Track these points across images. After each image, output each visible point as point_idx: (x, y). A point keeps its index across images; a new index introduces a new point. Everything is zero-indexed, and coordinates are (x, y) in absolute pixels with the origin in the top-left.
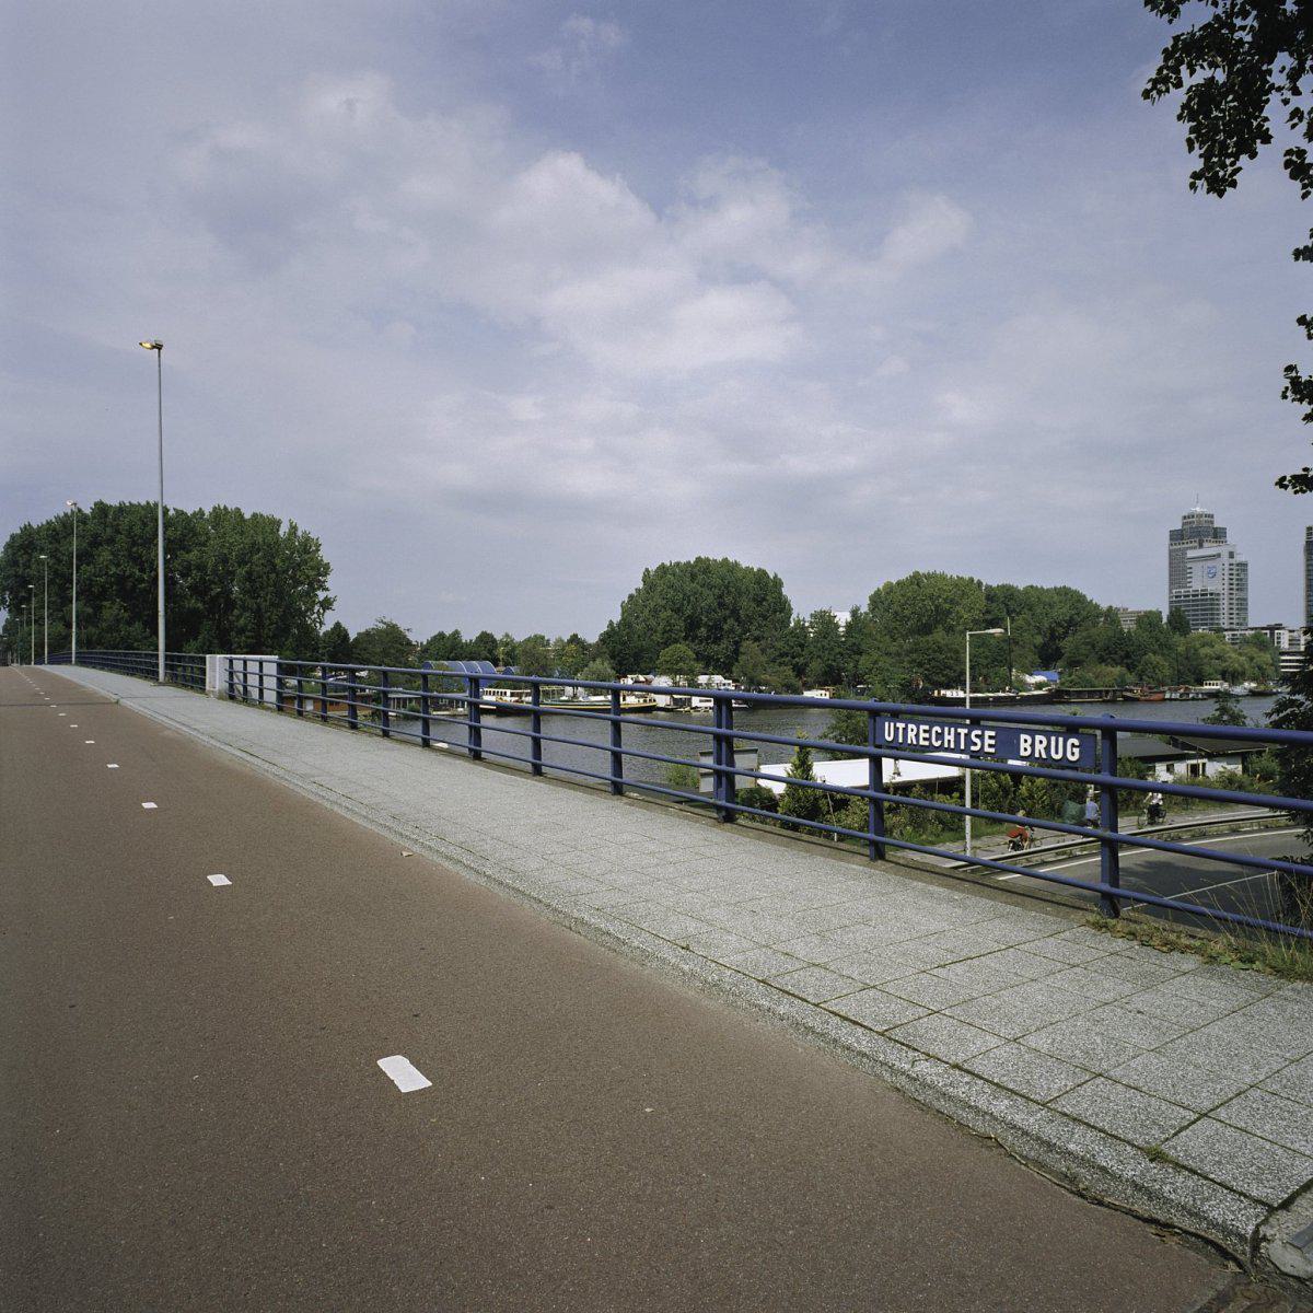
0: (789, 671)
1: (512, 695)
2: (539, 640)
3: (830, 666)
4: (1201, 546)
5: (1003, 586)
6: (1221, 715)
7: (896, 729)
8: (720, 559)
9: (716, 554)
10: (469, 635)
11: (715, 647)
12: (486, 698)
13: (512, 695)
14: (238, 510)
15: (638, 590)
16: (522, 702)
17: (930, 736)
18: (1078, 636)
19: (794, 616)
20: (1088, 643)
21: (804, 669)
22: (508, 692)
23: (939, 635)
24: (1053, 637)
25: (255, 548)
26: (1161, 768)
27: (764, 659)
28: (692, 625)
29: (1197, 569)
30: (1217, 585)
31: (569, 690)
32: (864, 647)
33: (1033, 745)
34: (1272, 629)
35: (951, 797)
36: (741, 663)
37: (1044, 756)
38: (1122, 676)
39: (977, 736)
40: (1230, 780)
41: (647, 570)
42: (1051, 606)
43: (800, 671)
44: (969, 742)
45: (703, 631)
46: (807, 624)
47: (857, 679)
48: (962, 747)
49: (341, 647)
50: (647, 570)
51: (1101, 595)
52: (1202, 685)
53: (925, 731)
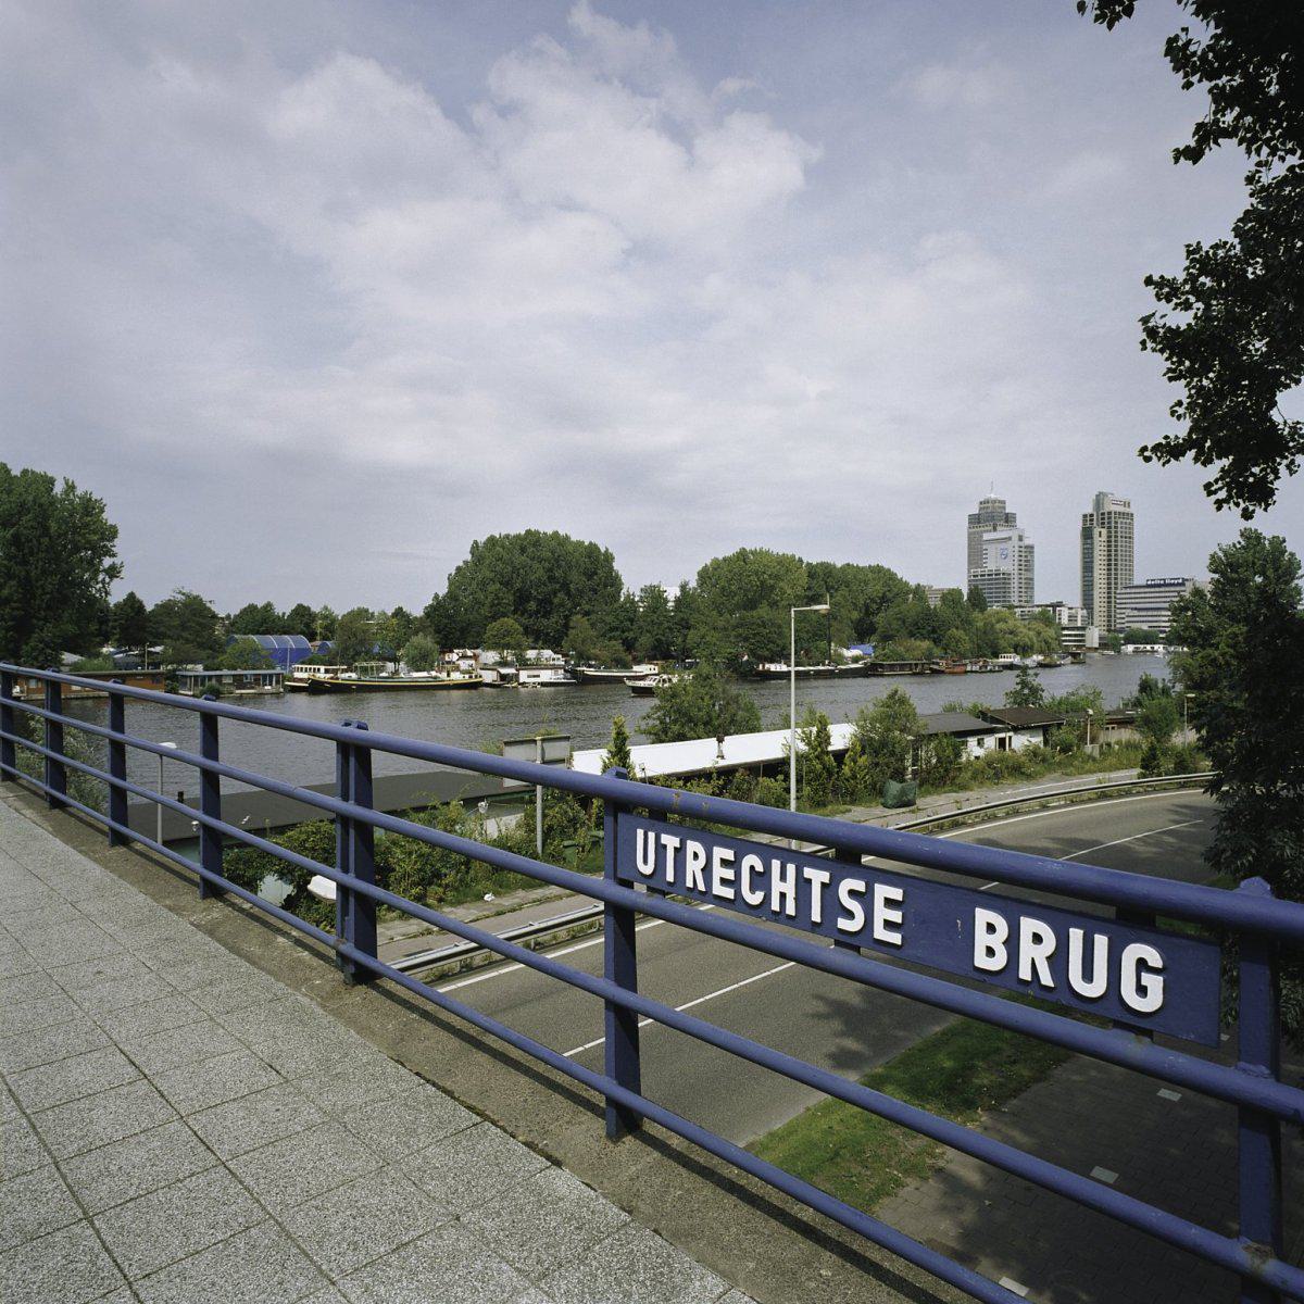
0: (617, 645)
1: (327, 671)
2: (363, 614)
3: (658, 640)
4: (995, 529)
5: (822, 564)
6: (1023, 688)
7: (661, 849)
8: (550, 532)
9: (546, 527)
10: (284, 608)
11: (545, 622)
12: (297, 675)
13: (327, 671)
15: (466, 562)
16: (337, 679)
17: (738, 875)
18: (891, 612)
19: (624, 591)
20: (898, 619)
21: (634, 644)
22: (322, 668)
23: (763, 611)
24: (868, 612)
25: (23, 508)
26: (972, 741)
27: (593, 633)
28: (522, 598)
29: (992, 551)
30: (1009, 566)
31: (390, 666)
32: (692, 622)
33: (1012, 943)
34: (1054, 606)
35: (776, 781)
36: (571, 637)
37: (1046, 979)
38: (929, 649)
39: (853, 893)
40: (1033, 753)
41: (476, 542)
42: (866, 583)
43: (629, 646)
44: (833, 907)
45: (532, 605)
46: (636, 599)
47: (686, 653)
48: (816, 917)
49: (134, 623)
50: (476, 542)
51: (910, 575)
52: (998, 658)
53: (725, 863)
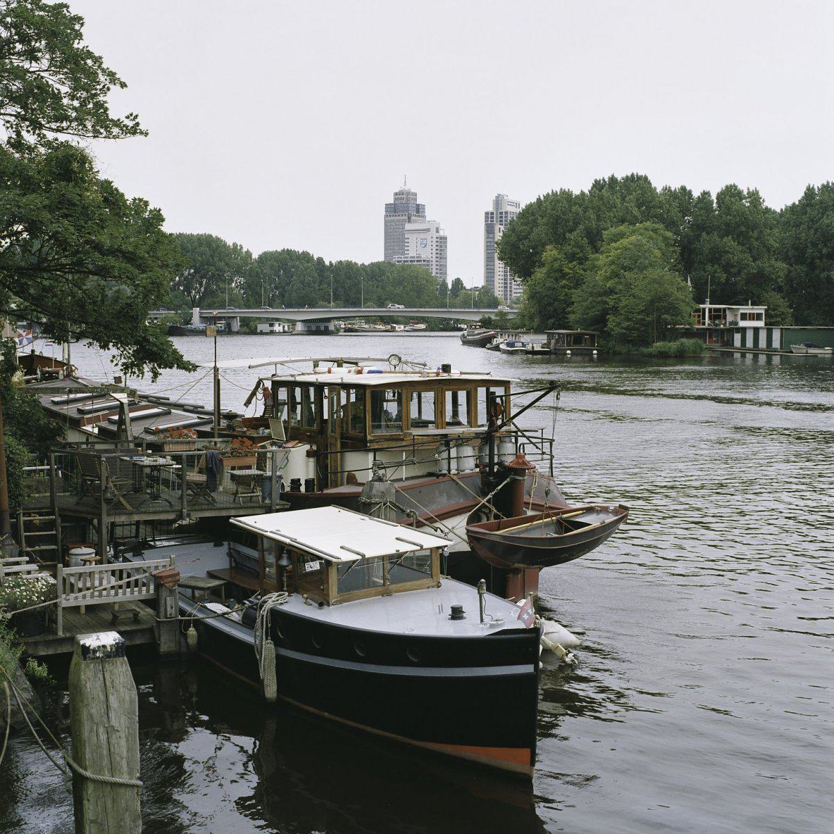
14: (683, 189)
